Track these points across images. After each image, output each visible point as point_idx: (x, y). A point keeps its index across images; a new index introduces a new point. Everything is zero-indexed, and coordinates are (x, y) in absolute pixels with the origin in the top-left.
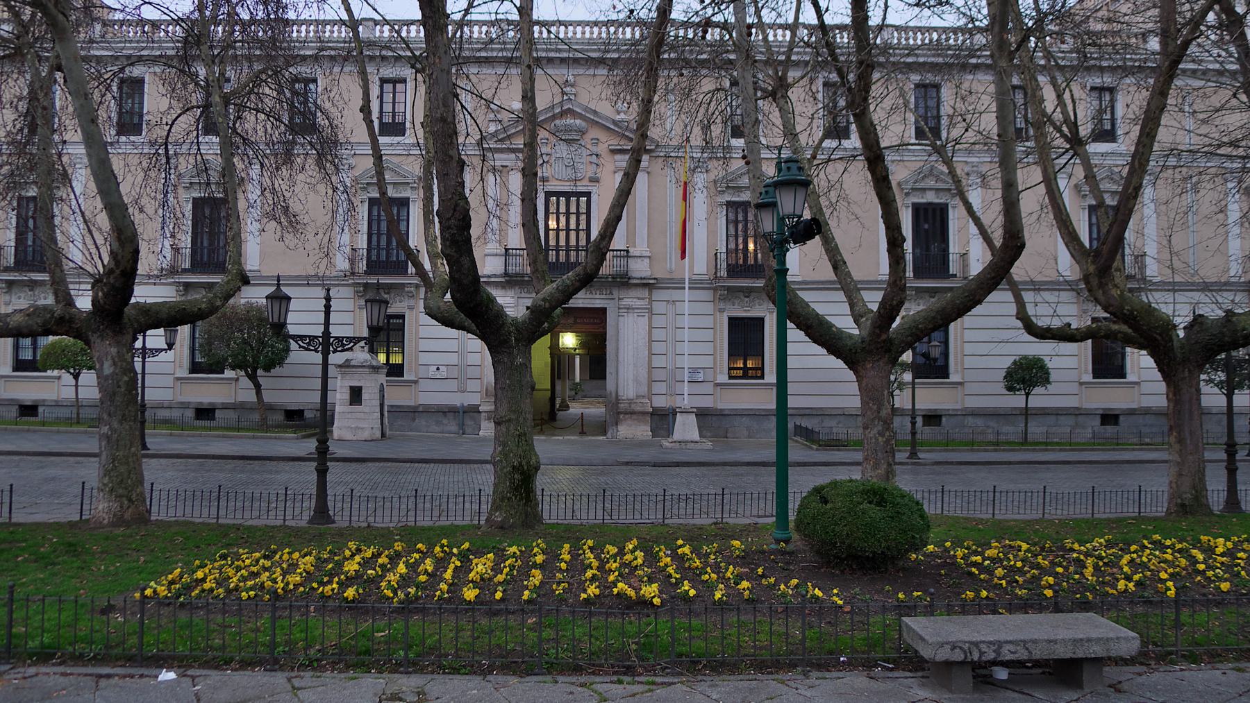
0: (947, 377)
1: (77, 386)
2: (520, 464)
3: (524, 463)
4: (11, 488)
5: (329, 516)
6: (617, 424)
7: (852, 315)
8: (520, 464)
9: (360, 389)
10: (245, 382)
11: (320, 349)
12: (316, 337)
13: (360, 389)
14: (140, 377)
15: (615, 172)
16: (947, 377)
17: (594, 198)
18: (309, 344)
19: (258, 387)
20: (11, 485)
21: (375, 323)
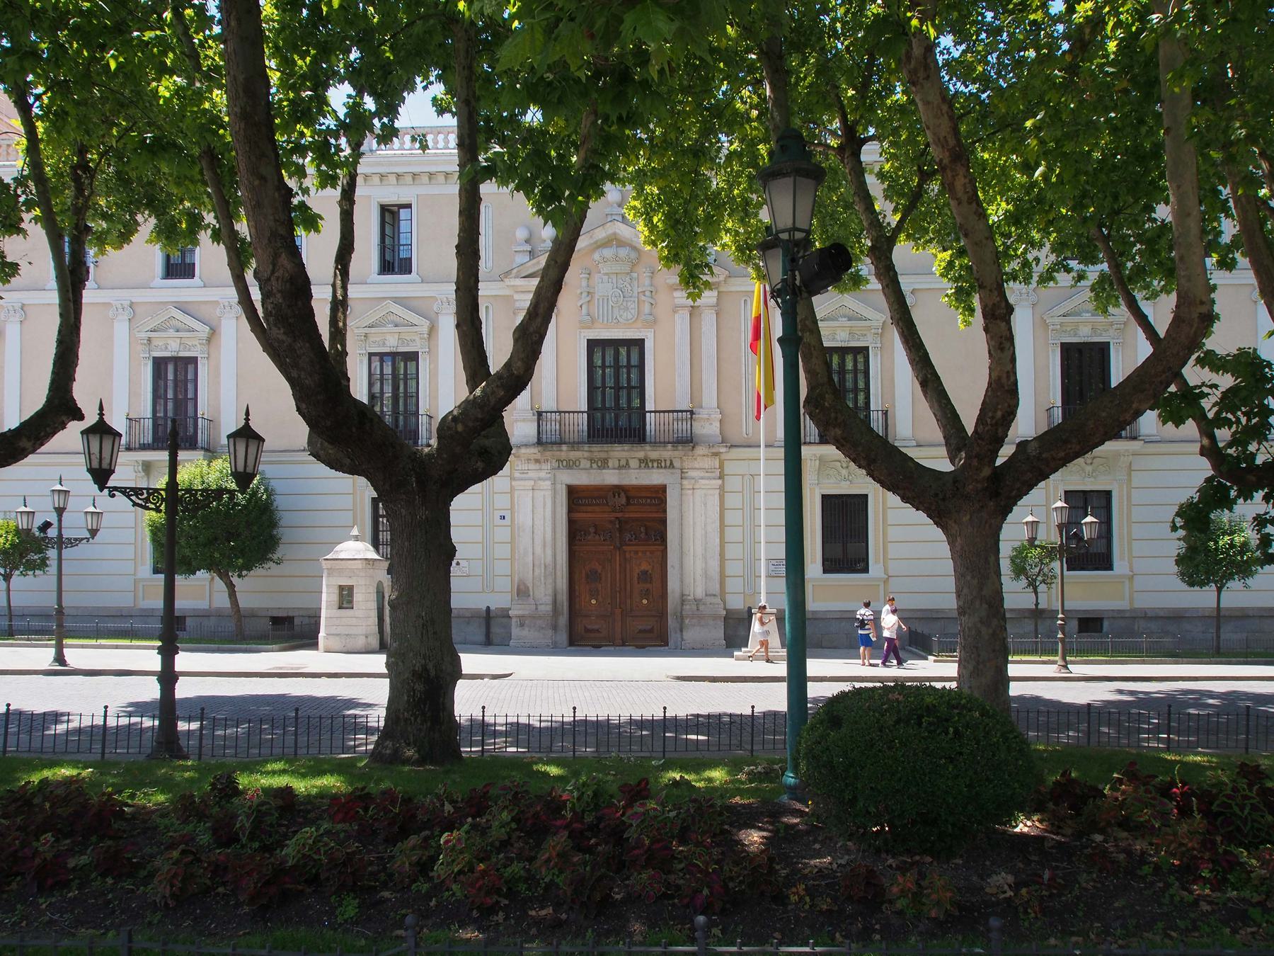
0: (1068, 570)
1: (8, 590)
2: (425, 669)
3: (430, 666)
4: (106, 712)
5: (180, 749)
6: (681, 631)
7: (896, 273)
8: (425, 669)
9: (351, 588)
10: (220, 584)
11: (163, 507)
12: (157, 490)
13: (351, 588)
14: (858, 685)
15: (675, 312)
16: (1068, 570)
17: (649, 346)
18: (147, 500)
19: (231, 586)
20: (106, 707)
21: (241, 469)
